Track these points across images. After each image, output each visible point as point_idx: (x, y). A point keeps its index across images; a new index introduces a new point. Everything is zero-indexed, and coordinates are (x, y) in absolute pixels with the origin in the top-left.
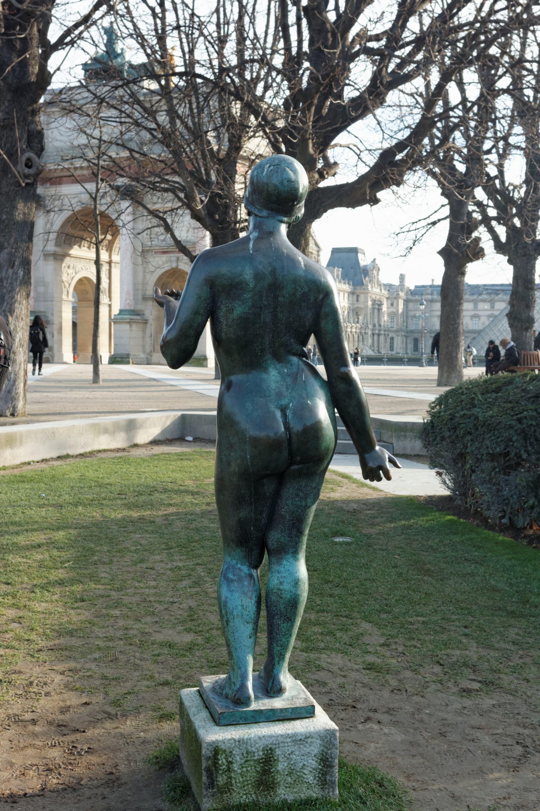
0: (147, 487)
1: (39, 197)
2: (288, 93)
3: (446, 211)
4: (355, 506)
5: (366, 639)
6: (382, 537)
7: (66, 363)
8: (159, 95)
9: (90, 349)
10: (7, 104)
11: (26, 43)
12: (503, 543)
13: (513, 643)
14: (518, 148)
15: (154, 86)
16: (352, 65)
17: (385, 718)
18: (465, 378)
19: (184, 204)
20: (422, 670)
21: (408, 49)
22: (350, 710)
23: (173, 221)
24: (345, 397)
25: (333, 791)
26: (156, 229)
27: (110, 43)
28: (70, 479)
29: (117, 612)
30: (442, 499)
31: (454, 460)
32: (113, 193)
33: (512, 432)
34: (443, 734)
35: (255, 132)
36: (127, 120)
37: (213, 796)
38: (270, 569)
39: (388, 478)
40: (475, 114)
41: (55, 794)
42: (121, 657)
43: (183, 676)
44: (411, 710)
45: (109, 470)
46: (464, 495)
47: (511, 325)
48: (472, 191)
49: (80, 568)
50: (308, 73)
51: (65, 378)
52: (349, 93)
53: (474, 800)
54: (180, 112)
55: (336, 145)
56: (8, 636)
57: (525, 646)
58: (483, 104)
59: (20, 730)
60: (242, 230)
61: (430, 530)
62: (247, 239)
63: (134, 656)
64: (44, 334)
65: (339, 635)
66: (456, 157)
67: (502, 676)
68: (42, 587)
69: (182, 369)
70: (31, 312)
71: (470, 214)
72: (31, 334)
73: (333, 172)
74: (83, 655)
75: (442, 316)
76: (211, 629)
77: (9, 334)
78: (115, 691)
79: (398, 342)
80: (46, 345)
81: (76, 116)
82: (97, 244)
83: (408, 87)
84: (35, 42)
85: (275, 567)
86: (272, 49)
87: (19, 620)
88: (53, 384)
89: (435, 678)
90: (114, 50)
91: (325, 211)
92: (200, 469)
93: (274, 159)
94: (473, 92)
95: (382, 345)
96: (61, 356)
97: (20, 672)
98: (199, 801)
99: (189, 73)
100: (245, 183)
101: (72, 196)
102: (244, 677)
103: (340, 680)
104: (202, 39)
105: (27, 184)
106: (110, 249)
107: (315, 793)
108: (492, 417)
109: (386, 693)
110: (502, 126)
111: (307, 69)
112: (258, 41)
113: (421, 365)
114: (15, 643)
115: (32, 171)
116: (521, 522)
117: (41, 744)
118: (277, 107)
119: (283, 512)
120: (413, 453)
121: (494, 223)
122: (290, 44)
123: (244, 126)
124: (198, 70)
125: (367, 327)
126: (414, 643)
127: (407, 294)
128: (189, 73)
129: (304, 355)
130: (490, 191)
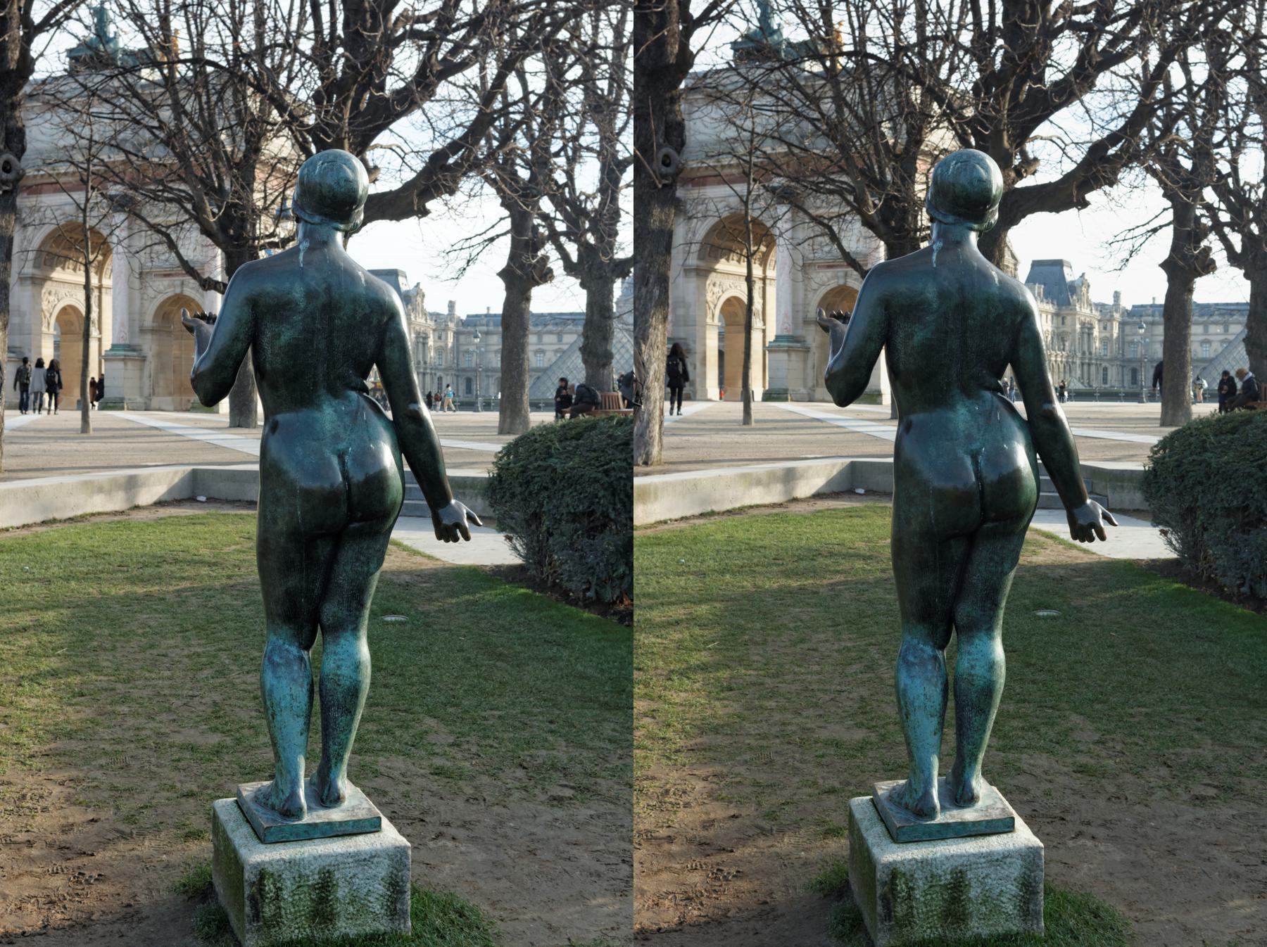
0: (810, 550)
2: (978, 75)
3: (507, 225)
4: (1062, 572)
6: (442, 616)
7: (710, 400)
8: (823, 78)
9: (740, 383)
11: (663, 19)
12: (589, 621)
14: (1255, 140)
15: (817, 68)
16: (1054, 43)
17: (1101, 833)
18: (1194, 417)
19: (853, 208)
20: (501, 774)
21: (1122, 23)
22: (1058, 822)
23: (178, 238)
24: (1049, 440)
25: (405, 923)
26: (820, 239)
27: (765, 18)
28: (715, 541)
29: (125, 709)
31: (527, 521)
32: (768, 195)
33: (1251, 481)
34: (1171, 852)
35: (939, 122)
36: (785, 109)
37: (890, 930)
38: (958, 649)
39: (1103, 538)
40: (1202, 100)
41: (696, 929)
42: (776, 758)
43: (854, 781)
44: (492, 823)
46: (1195, 558)
47: (1249, 353)
48: (1200, 192)
49: (77, 656)
50: (1001, 52)
51: (48, 427)
52: (1051, 76)
53: (575, 931)
54: (848, 99)
55: (376, 146)
58: (1212, 88)
59: (12, 853)
60: (924, 239)
61: (500, 606)
62: (929, 250)
63: (149, 762)
64: (684, 365)
66: (1181, 151)
68: (682, 674)
69: (852, 407)
70: (669, 339)
71: (1198, 219)
73: (1032, 169)
74: (87, 761)
76: (888, 724)
78: (770, 801)
79: (1113, 373)
81: (723, 104)
82: (749, 257)
83: (1121, 68)
84: (675, 17)
85: (966, 648)
86: (958, 23)
88: (694, 426)
89: (518, 784)
90: (769, 26)
91: (1024, 216)
92: (873, 528)
93: (962, 154)
94: (1200, 74)
95: (1093, 377)
96: (705, 391)
97: (654, 778)
98: (240, 938)
99: (860, 53)
100: (927, 183)
101: (55, 207)
102: (928, 783)
103: (1045, 786)
104: (874, 12)
105: (664, 185)
106: (764, 263)
107: (1015, 926)
108: (572, 468)
109: (460, 803)
110: (1235, 114)
111: (1001, 47)
112: (942, 14)
113: (1141, 401)
114: (647, 743)
115: (670, 170)
119: (340, 580)
120: (1131, 508)
121: (1227, 230)
123: (925, 116)
124: (871, 49)
125: (1074, 356)
127: (457, 325)
128: (860, 53)
129: (1000, 390)
130: (1222, 192)
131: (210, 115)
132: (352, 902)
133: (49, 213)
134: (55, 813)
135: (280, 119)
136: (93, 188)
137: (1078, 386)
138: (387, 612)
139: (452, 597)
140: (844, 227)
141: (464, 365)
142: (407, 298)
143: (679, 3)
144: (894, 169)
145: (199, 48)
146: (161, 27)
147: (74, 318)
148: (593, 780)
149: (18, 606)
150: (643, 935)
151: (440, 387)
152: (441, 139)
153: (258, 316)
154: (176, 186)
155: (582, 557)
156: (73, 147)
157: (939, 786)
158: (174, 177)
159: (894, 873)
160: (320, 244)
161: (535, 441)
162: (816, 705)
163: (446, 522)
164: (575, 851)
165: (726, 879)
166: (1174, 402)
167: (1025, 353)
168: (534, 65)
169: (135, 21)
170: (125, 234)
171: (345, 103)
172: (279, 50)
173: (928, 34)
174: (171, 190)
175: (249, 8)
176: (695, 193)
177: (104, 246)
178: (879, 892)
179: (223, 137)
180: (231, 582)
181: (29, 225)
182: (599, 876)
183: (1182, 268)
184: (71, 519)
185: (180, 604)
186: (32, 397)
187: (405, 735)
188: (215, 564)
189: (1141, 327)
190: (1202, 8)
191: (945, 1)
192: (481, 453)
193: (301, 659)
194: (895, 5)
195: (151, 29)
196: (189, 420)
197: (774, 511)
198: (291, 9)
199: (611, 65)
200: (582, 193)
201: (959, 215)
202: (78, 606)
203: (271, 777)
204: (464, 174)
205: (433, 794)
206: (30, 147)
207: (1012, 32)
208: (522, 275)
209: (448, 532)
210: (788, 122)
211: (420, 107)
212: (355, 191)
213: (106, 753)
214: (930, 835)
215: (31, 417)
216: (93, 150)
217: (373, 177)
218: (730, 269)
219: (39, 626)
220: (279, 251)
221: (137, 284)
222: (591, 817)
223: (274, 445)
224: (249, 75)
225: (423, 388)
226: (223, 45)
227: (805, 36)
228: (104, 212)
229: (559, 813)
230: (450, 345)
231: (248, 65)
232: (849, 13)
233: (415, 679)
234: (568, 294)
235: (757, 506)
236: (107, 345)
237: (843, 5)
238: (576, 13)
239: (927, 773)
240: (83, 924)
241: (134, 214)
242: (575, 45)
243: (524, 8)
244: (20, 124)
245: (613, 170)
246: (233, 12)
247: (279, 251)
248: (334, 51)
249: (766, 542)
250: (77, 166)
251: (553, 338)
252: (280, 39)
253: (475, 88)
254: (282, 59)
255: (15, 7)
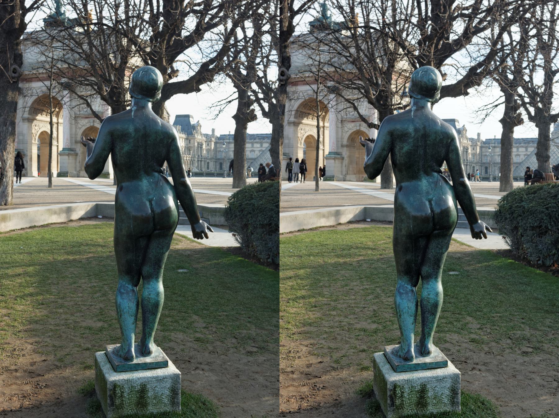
0: (78, 243)
1: (20, 88)
2: (152, 33)
3: (503, 99)
4: (189, 253)
5: (470, 326)
6: (475, 272)
7: (34, 177)
8: (84, 35)
9: (47, 169)
10: (3, 40)
11: (13, 8)
12: (539, 274)
13: (275, 326)
14: (274, 62)
15: (81, 30)
16: (186, 19)
17: (206, 367)
18: (247, 184)
20: (501, 342)
21: (215, 10)
22: (188, 363)
23: (358, 105)
24: (183, 194)
26: (82, 105)
27: (58, 8)
28: (305, 242)
29: (334, 313)
30: (236, 249)
31: (512, 230)
32: (59, 86)
33: (543, 214)
34: (237, 376)
35: (135, 54)
36: (67, 48)
37: (393, 411)
38: (143, 287)
39: (207, 237)
40: (251, 44)
41: (27, 410)
42: (338, 337)
43: (373, 346)
44: (497, 363)
45: (326, 237)
46: (248, 246)
48: (250, 85)
49: (313, 289)
50: (162, 23)
51: (300, 188)
52: (184, 33)
53: (533, 411)
54: (95, 44)
55: (445, 65)
56: (2, 324)
57: (555, 328)
58: (255, 39)
59: (9, 375)
60: (128, 105)
61: (500, 267)
62: (131, 110)
64: (22, 161)
65: (181, 322)
66: (241, 66)
67: (269, 344)
69: (96, 180)
70: (16, 150)
71: (249, 97)
72: (15, 161)
73: (176, 75)
74: (318, 336)
75: (235, 151)
76: (112, 319)
77: (4, 162)
79: (212, 165)
80: (24, 167)
81: (40, 46)
82: (51, 114)
83: (215, 30)
84: (18, 7)
85: (146, 286)
86: (143, 10)
87: (8, 315)
88: (294, 192)
90: (60, 11)
91: (172, 95)
92: (106, 233)
93: (145, 68)
94: (250, 33)
95: (203, 166)
96: (32, 173)
97: (9, 343)
98: (385, 414)
99: (100, 23)
100: (129, 81)
102: (130, 346)
103: (182, 347)
104: (106, 5)
105: (14, 82)
106: (57, 116)
107: (168, 409)
108: (532, 207)
109: (482, 355)
110: (265, 50)
111: (162, 21)
112: (136, 6)
113: (224, 177)
114: (6, 328)
115: (16, 75)
116: (548, 263)
117: (297, 384)
118: (146, 41)
120: (220, 224)
121: (262, 101)
122: (153, 8)
123: (129, 51)
124: (105, 22)
126: (222, 326)
128: (100, 23)
129: (162, 172)
130: (260, 85)
131: (372, 51)
132: (435, 398)
133: (301, 94)
134: (304, 359)
135: (403, 53)
136: (320, 83)
137: (196, 170)
138: (450, 270)
139: (479, 263)
140: (93, 100)
141: (484, 161)
142: (459, 132)
143: (20, 1)
144: (115, 75)
145: (367, 21)
146: (351, 12)
147: (312, 140)
148: (541, 344)
149: (288, 268)
150: (283, 414)
151: (474, 171)
152: (474, 62)
153: (393, 140)
154: (357, 82)
155: (536, 246)
156: (312, 65)
157: (135, 347)
158: (356, 78)
159: (115, 385)
160: (421, 108)
161: (516, 195)
162: (81, 311)
163: (476, 230)
164: (533, 376)
165: (41, 388)
166: (238, 177)
167: (173, 156)
168: (515, 29)
169: (339, 9)
170: (334, 103)
171: (432, 46)
172: (402, 22)
173: (130, 15)
174: (355, 84)
175: (389, 4)
176: (27, 85)
177: (325, 109)
178: (108, 394)
179: (378, 60)
180: (382, 257)
181: (292, 99)
182: (544, 386)
183: (242, 118)
184: (311, 229)
185: (359, 267)
186: (294, 175)
187: (458, 325)
188: (374, 249)
189: (224, 144)
190: (251, 3)
191: (137, 1)
192: (492, 200)
193: (412, 291)
194: (115, 2)
195: (346, 13)
196: (363, 185)
197: (62, 226)
198: (408, 4)
199: (549, 29)
200: (536, 85)
201: (144, 95)
202: (314, 267)
203: (399, 343)
204: (484, 77)
205: (471, 350)
206: (293, 65)
207: (167, 14)
208: (510, 121)
209: (477, 235)
210: (68, 54)
211: (465, 47)
212: (436, 84)
213: (326, 332)
214: (131, 368)
215: (293, 184)
216: (321, 66)
217: (444, 78)
218: (43, 119)
219: (297, 276)
220: (402, 111)
221: (340, 125)
222: (540, 360)
223: (400, 197)
224: (389, 33)
225: (466, 171)
226: (378, 20)
227: (76, 16)
228: (325, 93)
229: (526, 359)
230: (478, 152)
231: (389, 29)
232: (95, 6)
233: (463, 300)
234: (530, 130)
235: (55, 223)
236: (327, 152)
237: (92, 2)
238: (534, 6)
239: (129, 341)
240: (316, 408)
241: (339, 94)
242: (533, 20)
243: (511, 3)
244: (288, 55)
245: (550, 75)
246: (382, 6)
247: (402, 111)
248: (427, 22)
249: (58, 239)
250: (314, 73)
251: (524, 149)
252: (403, 17)
253: (489, 39)
254: (404, 26)
255: (286, 3)
